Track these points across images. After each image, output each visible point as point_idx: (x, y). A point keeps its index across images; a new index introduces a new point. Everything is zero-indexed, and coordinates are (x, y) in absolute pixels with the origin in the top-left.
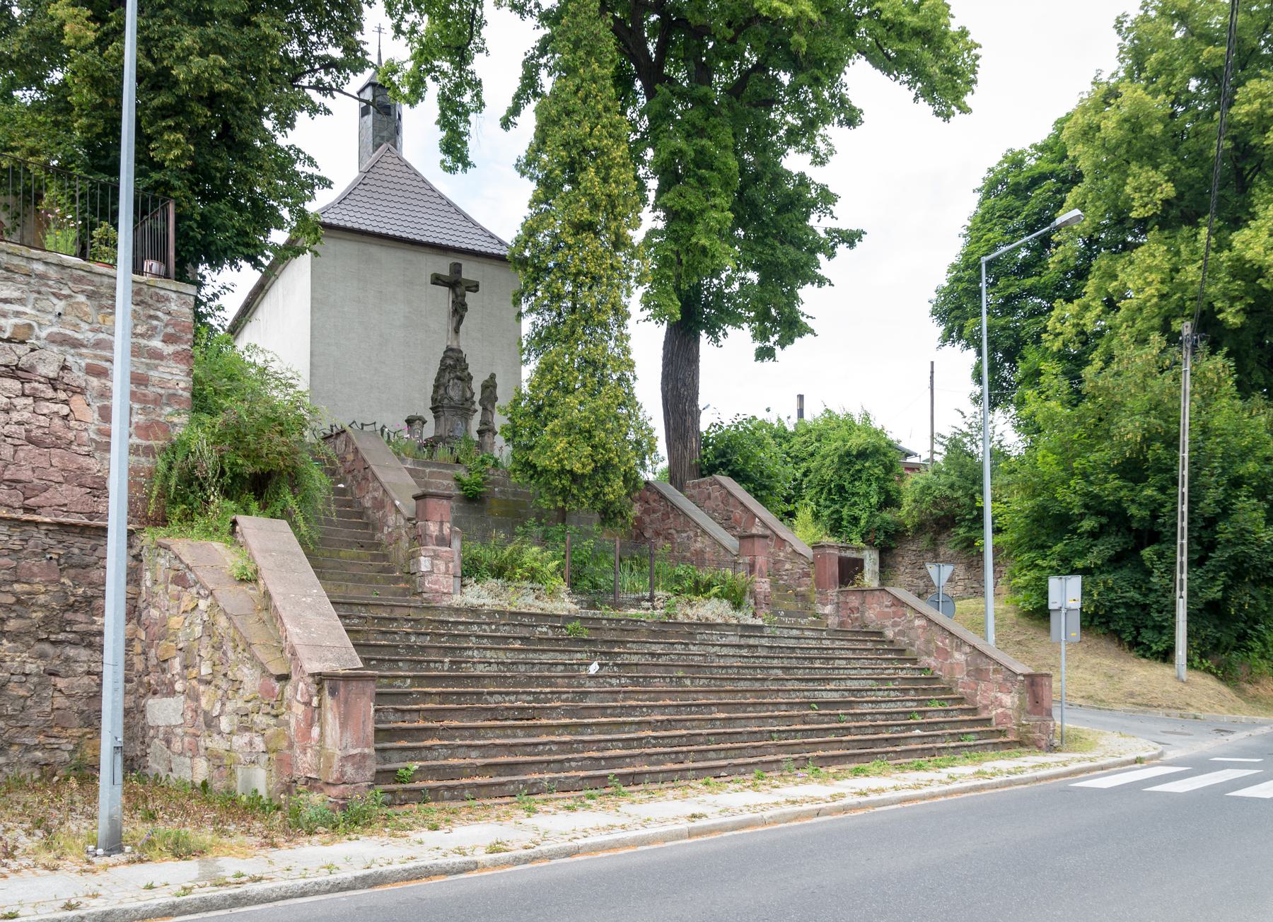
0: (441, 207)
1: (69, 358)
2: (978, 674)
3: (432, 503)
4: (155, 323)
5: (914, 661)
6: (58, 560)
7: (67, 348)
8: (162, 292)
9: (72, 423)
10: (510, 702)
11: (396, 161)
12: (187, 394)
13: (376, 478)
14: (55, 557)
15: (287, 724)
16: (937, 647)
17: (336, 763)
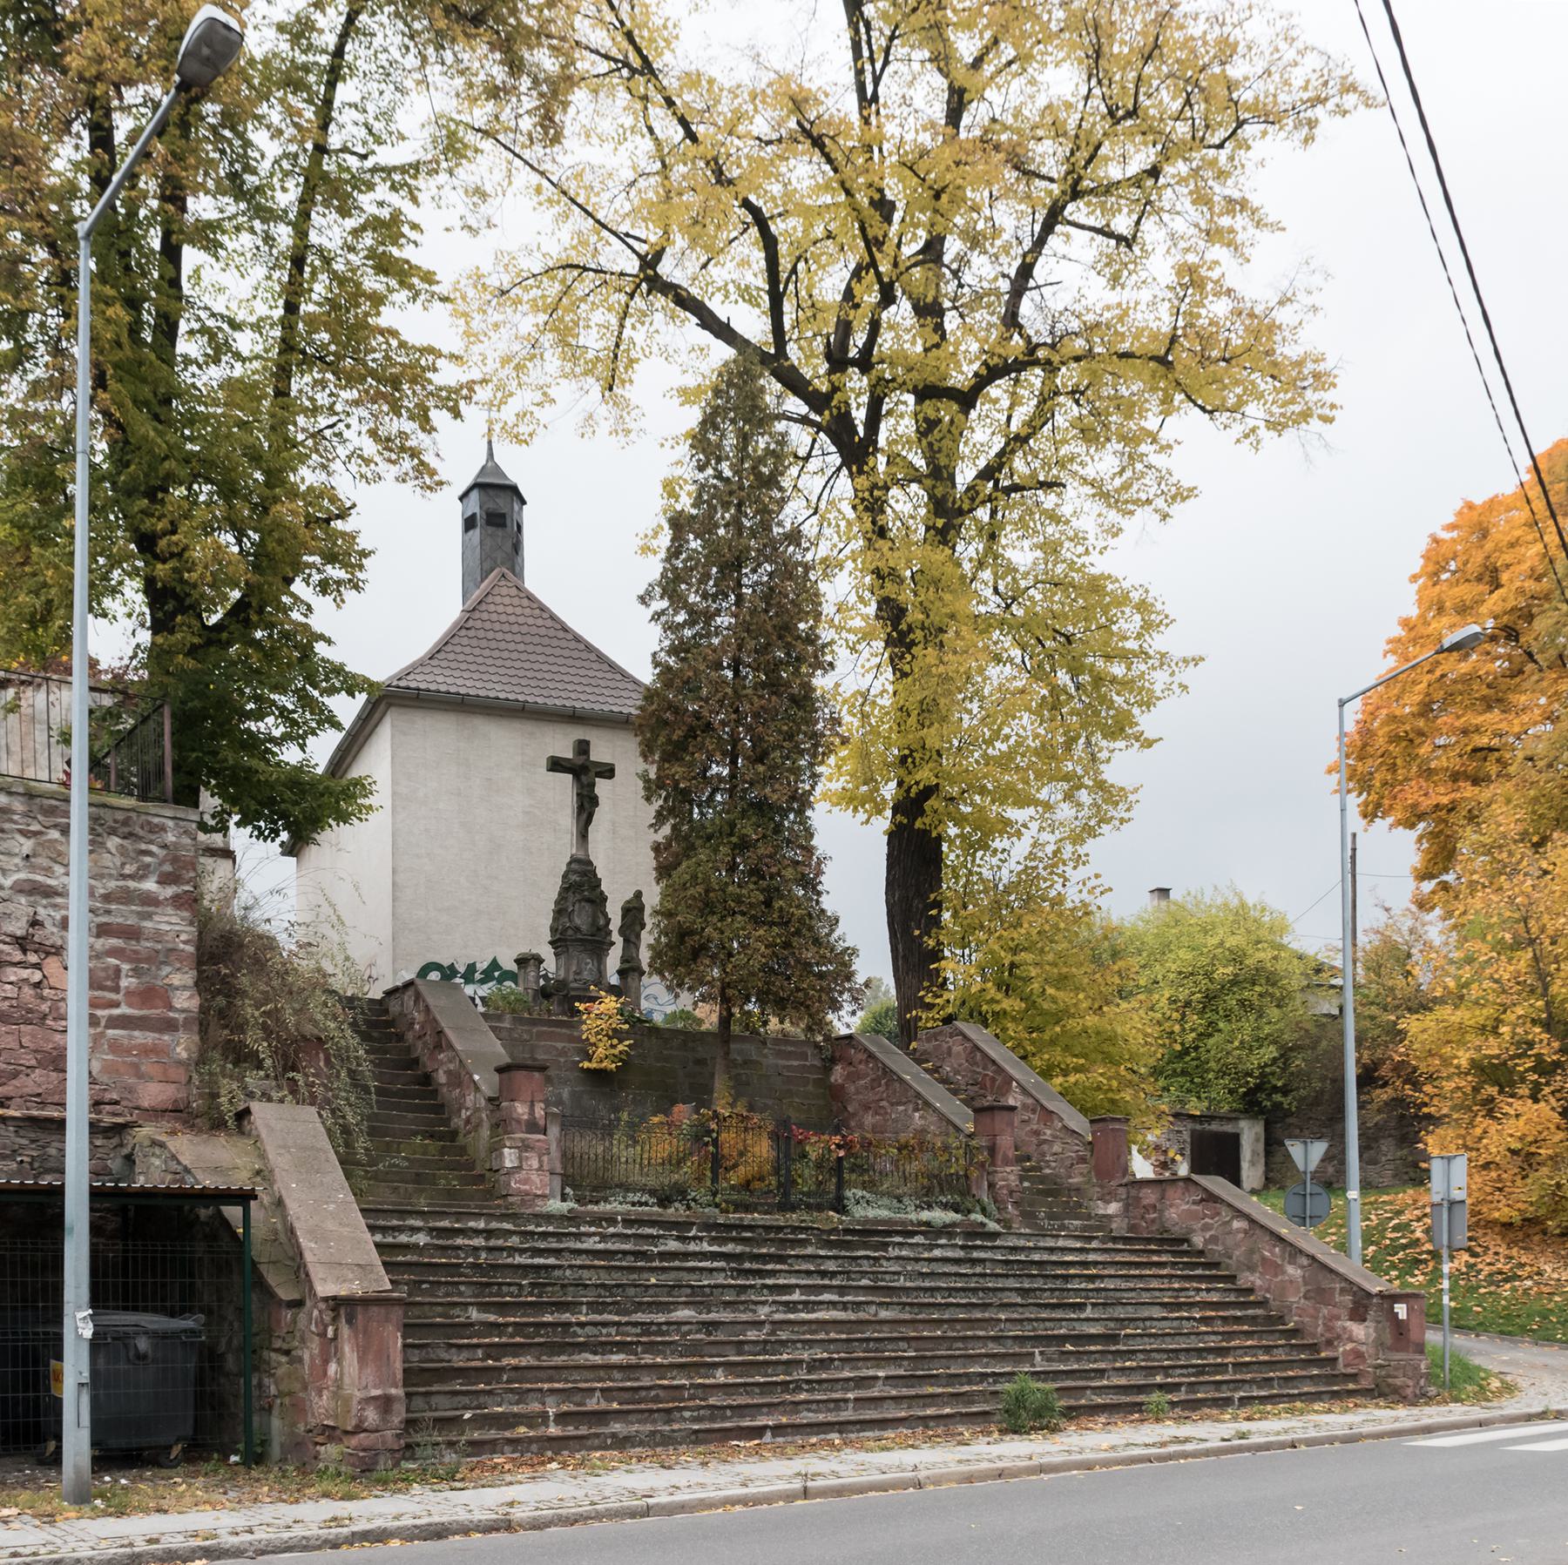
0: (576, 654)
1: (41, 910)
2: (1319, 1295)
3: (520, 1076)
4: (148, 859)
5: (1232, 1278)
6: (31, 1164)
7: (38, 898)
8: (156, 820)
9: (46, 992)
10: (609, 1335)
11: (514, 592)
12: (190, 949)
13: (451, 1047)
14: (26, 1159)
15: (300, 1360)
16: (1264, 1259)
17: (355, 1407)
